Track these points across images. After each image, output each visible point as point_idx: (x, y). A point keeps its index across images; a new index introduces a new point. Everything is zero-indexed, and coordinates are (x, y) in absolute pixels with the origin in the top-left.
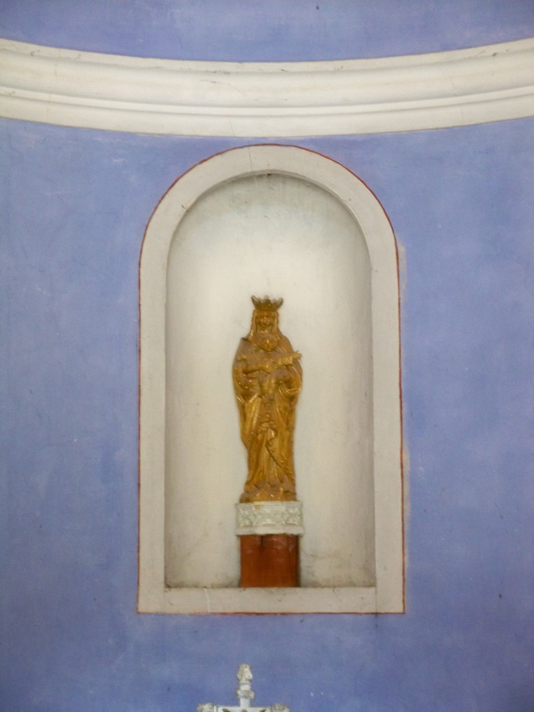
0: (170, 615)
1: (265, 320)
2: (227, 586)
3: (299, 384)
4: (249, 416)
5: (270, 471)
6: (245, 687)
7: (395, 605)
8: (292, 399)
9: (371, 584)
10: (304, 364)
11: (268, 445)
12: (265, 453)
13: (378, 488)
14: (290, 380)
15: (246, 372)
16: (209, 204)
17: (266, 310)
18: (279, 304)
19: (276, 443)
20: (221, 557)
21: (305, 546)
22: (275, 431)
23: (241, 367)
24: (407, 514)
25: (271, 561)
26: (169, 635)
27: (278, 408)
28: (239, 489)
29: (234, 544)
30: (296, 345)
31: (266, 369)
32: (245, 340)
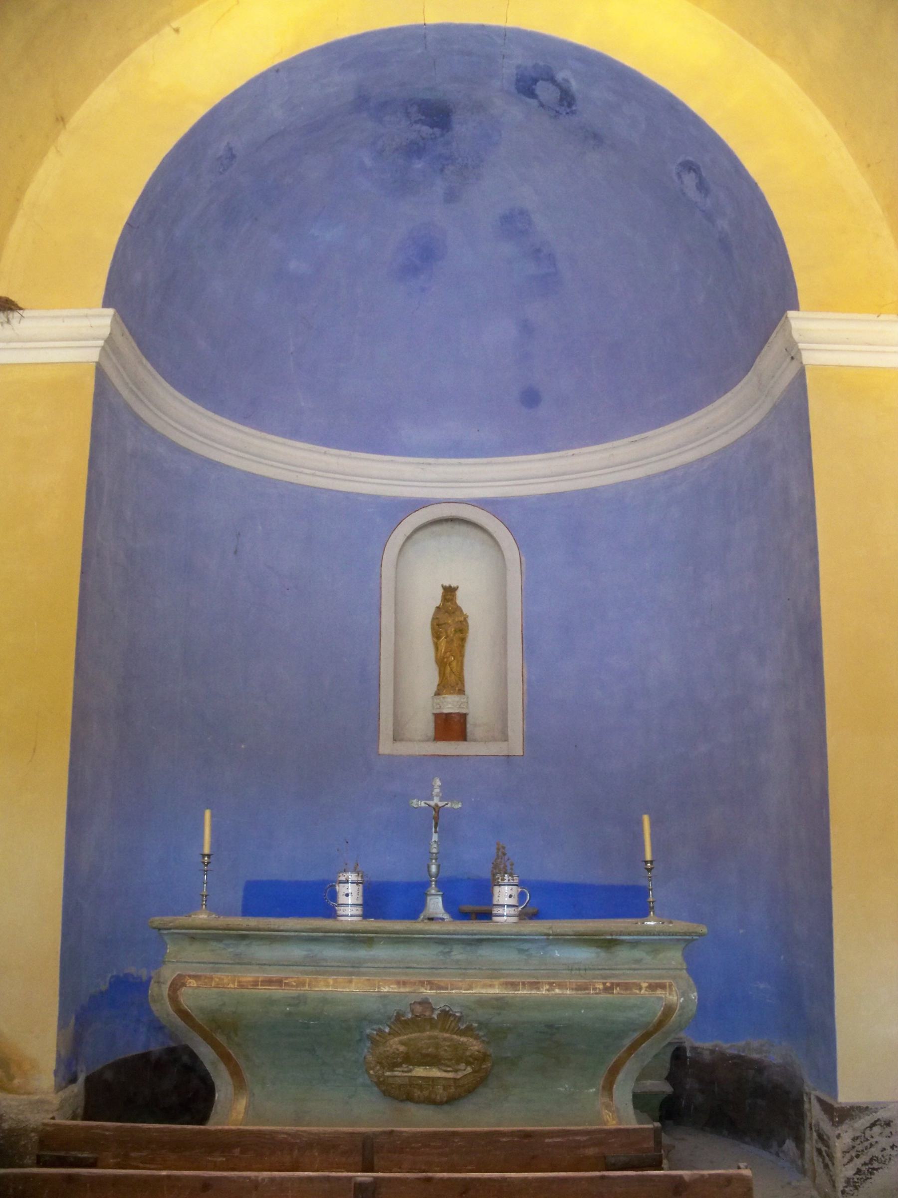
2: (428, 741)
4: (440, 648)
5: (451, 678)
6: (437, 790)
8: (463, 640)
10: (470, 622)
11: (450, 665)
12: (448, 669)
14: (462, 629)
15: (438, 625)
16: (417, 536)
17: (449, 592)
19: (454, 664)
20: (422, 722)
21: (470, 720)
25: (451, 727)
28: (434, 688)
29: (431, 718)
32: (438, 608)
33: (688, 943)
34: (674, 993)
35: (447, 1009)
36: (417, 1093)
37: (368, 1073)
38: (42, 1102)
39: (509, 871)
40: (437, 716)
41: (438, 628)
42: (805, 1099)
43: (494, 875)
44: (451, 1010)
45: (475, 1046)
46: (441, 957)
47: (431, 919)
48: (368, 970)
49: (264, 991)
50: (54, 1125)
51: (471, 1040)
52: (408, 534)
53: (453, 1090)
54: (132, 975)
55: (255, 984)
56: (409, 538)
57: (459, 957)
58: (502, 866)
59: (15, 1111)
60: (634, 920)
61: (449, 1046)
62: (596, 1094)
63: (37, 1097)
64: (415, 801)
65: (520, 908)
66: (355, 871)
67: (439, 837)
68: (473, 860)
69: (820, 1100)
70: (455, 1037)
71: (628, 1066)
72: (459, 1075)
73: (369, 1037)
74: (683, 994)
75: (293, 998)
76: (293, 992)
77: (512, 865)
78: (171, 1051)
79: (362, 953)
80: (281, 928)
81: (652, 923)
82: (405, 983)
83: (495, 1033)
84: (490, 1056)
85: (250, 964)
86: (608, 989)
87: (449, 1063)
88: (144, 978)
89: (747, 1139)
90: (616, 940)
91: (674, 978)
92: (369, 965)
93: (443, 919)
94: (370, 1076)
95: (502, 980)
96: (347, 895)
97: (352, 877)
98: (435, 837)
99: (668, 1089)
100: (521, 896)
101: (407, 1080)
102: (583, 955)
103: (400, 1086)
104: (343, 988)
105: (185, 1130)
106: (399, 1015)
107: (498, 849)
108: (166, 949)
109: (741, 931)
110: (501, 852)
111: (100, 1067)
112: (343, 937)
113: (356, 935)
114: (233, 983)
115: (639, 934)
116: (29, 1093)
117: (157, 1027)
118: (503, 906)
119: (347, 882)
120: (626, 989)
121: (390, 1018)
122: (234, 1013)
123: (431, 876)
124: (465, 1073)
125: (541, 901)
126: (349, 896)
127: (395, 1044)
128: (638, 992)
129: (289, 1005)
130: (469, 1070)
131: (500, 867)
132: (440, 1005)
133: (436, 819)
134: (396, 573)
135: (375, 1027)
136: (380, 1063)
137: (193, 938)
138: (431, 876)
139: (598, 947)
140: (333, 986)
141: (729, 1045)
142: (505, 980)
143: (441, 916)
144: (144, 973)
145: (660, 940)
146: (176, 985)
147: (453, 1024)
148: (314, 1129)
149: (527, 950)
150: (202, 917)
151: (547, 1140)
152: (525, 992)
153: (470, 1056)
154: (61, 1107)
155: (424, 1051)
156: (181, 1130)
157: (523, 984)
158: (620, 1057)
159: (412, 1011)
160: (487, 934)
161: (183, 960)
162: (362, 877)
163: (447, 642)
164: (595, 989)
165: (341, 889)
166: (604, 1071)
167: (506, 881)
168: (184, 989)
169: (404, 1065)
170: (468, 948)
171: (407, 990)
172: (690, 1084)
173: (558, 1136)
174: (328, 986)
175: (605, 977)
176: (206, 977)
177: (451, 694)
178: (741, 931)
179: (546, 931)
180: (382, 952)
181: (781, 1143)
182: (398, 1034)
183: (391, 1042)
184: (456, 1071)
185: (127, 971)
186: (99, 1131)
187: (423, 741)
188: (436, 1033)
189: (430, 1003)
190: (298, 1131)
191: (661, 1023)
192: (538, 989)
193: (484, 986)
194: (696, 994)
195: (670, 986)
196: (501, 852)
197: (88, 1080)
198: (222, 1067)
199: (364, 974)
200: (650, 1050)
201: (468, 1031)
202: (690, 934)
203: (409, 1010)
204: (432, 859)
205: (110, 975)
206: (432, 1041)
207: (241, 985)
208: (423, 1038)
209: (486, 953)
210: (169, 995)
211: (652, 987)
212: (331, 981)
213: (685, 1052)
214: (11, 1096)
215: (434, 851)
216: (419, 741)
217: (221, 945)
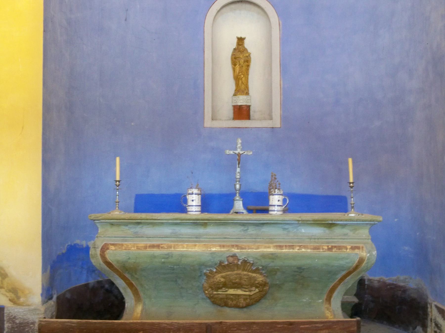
0: (213, 128)
1: (240, 43)
2: (230, 120)
3: (250, 62)
4: (236, 71)
5: (242, 88)
6: (239, 145)
7: (278, 125)
8: (248, 66)
9: (271, 119)
10: (252, 56)
11: (241, 79)
12: (240, 82)
13: (273, 91)
14: (248, 61)
15: (235, 58)
16: (224, 10)
17: (241, 40)
18: (244, 39)
19: (244, 79)
20: (227, 111)
21: (252, 109)
22: (243, 75)
23: (234, 56)
24: (282, 103)
25: (242, 112)
26: (214, 133)
27: (244, 68)
28: (233, 92)
29: (231, 108)
30: (249, 51)
31: (240, 56)
32: (235, 49)
33: (372, 226)
34: (364, 251)
35: (246, 259)
36: (230, 302)
37: (205, 292)
38: (35, 309)
39: (278, 187)
40: (235, 107)
41: (235, 60)
42: (429, 306)
43: (270, 190)
44: (248, 260)
45: (260, 278)
46: (242, 233)
47: (237, 213)
48: (203, 239)
49: (150, 251)
50: (46, 321)
51: (258, 275)
52: (218, 9)
53: (248, 301)
54: (78, 245)
55: (146, 247)
56: (219, 11)
57: (252, 232)
58: (274, 185)
59: (22, 314)
60: (344, 213)
61: (247, 278)
62: (322, 302)
63: (33, 307)
64: (228, 151)
65: (283, 207)
66: (197, 188)
67: (241, 170)
68: (257, 184)
69: (436, 307)
70: (250, 274)
71: (339, 287)
72: (252, 293)
73: (205, 274)
74: (369, 252)
75: (166, 255)
76: (165, 251)
77: (280, 184)
78: (99, 282)
79: (201, 230)
80: (159, 218)
81: (353, 215)
82: (224, 246)
83: (271, 272)
84: (268, 283)
85: (142, 237)
86: (330, 249)
87: (246, 287)
88: (84, 246)
89: (397, 326)
90: (334, 224)
91: (364, 244)
92: (205, 237)
93: (243, 213)
94: (206, 294)
95: (275, 244)
96: (193, 201)
97: (195, 191)
98: (238, 170)
99: (356, 300)
100: (284, 200)
101: (225, 296)
102: (317, 231)
103: (221, 299)
104: (192, 249)
105: (114, 323)
106: (221, 263)
107: (272, 176)
108: (98, 230)
109: (396, 220)
110: (274, 177)
111: (63, 291)
112: (191, 223)
113: (198, 221)
114: (134, 247)
115: (346, 221)
116: (29, 305)
117: (92, 270)
118: (275, 205)
119: (192, 194)
120: (339, 249)
121: (216, 264)
122: (135, 262)
123: (236, 190)
124: (255, 292)
125: (297, 203)
126: (194, 201)
127: (219, 278)
128: (345, 250)
129: (163, 258)
130: (257, 290)
131: (272, 186)
132: (242, 257)
133: (239, 161)
134: (212, 29)
135: (208, 269)
136: (211, 287)
137: (112, 224)
138: (236, 190)
139: (325, 227)
140: (186, 248)
141: (388, 278)
142: (275, 244)
143: (242, 211)
144: (84, 243)
145: (357, 224)
146: (104, 249)
147: (249, 267)
148: (181, 321)
149: (287, 229)
150: (117, 213)
151: (302, 326)
152: (287, 250)
153: (258, 283)
154: (45, 311)
155: (234, 281)
156: (111, 323)
157: (286, 246)
158: (335, 284)
159: (228, 260)
160: (266, 221)
161: (108, 236)
162: (201, 191)
163: (240, 67)
164: (323, 249)
165: (190, 198)
166: (327, 290)
167: (276, 193)
168: (108, 251)
169: (223, 288)
170: (257, 228)
171: (225, 249)
172: (367, 297)
173: (307, 324)
174: (183, 248)
175: (328, 243)
176: (119, 245)
177: (241, 95)
178: (396, 220)
179: (298, 219)
180: (211, 230)
181: (415, 328)
182: (221, 273)
183: (217, 276)
184: (250, 291)
185: (75, 242)
186: (68, 324)
187: (228, 120)
188: (239, 272)
189: (237, 256)
190: (172, 322)
191: (357, 267)
192: (293, 249)
193: (266, 247)
194: (376, 252)
195: (362, 248)
196: (274, 177)
197: (58, 298)
198: (129, 290)
199: (202, 242)
200: (352, 281)
201: (257, 271)
202: (373, 221)
203: (226, 260)
204: (237, 181)
205: (67, 245)
206: (238, 276)
207: (138, 248)
208: (233, 274)
209: (266, 230)
210: (100, 254)
211: (353, 248)
212: (185, 246)
213: (365, 282)
214: (19, 307)
215: (238, 177)
216: (225, 120)
217: (127, 228)
